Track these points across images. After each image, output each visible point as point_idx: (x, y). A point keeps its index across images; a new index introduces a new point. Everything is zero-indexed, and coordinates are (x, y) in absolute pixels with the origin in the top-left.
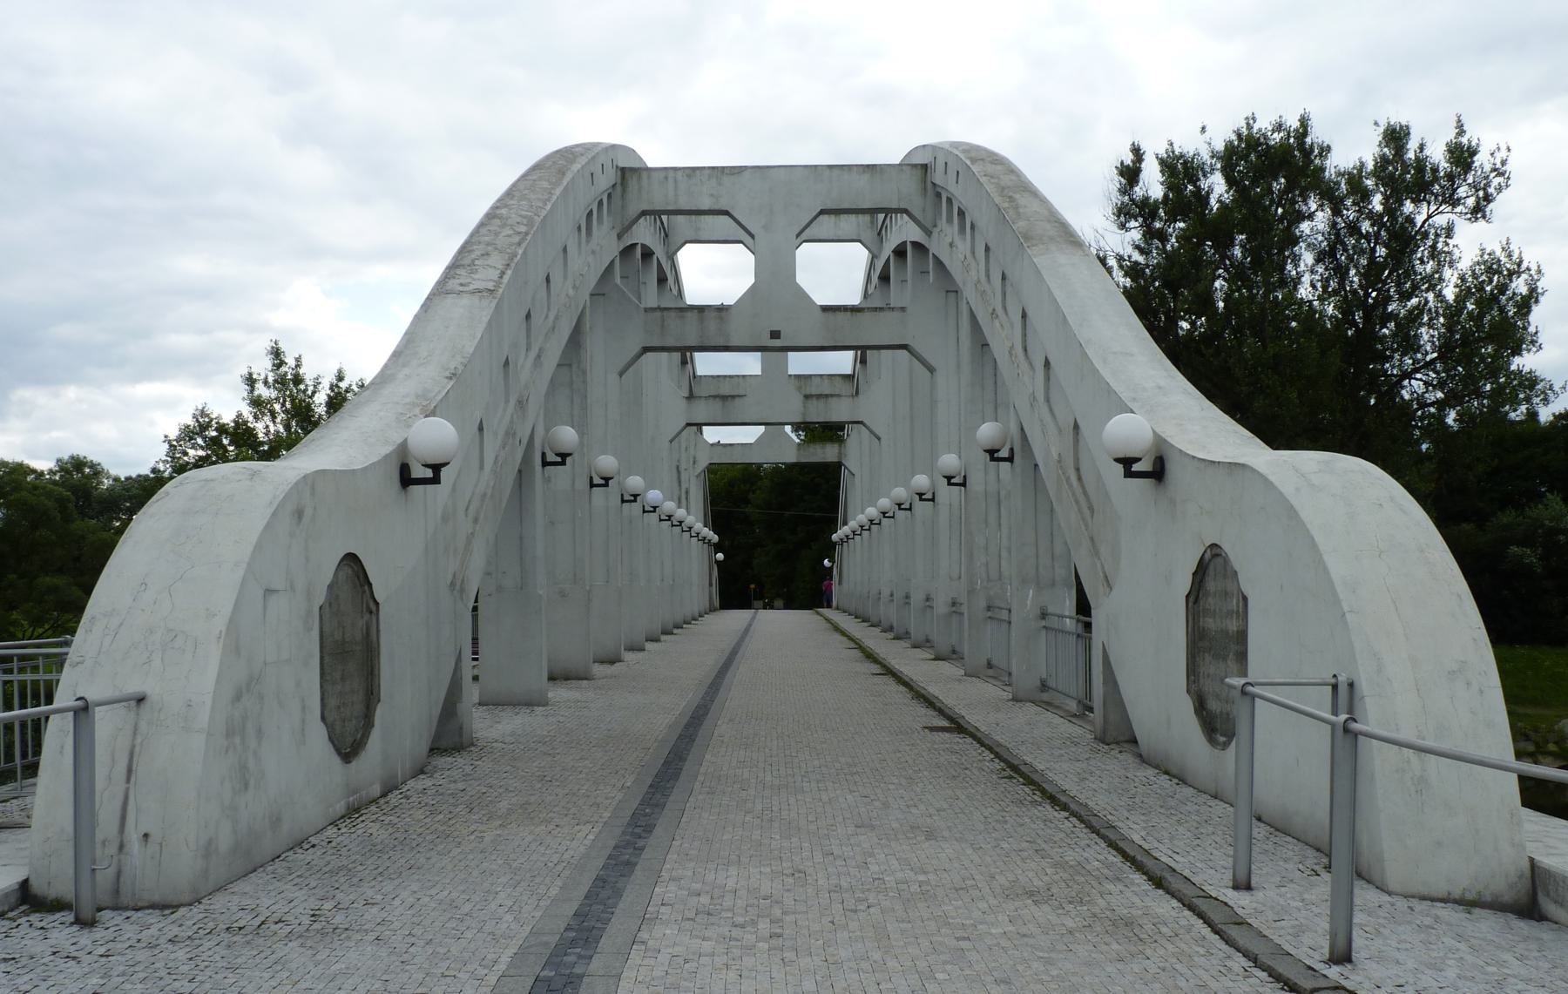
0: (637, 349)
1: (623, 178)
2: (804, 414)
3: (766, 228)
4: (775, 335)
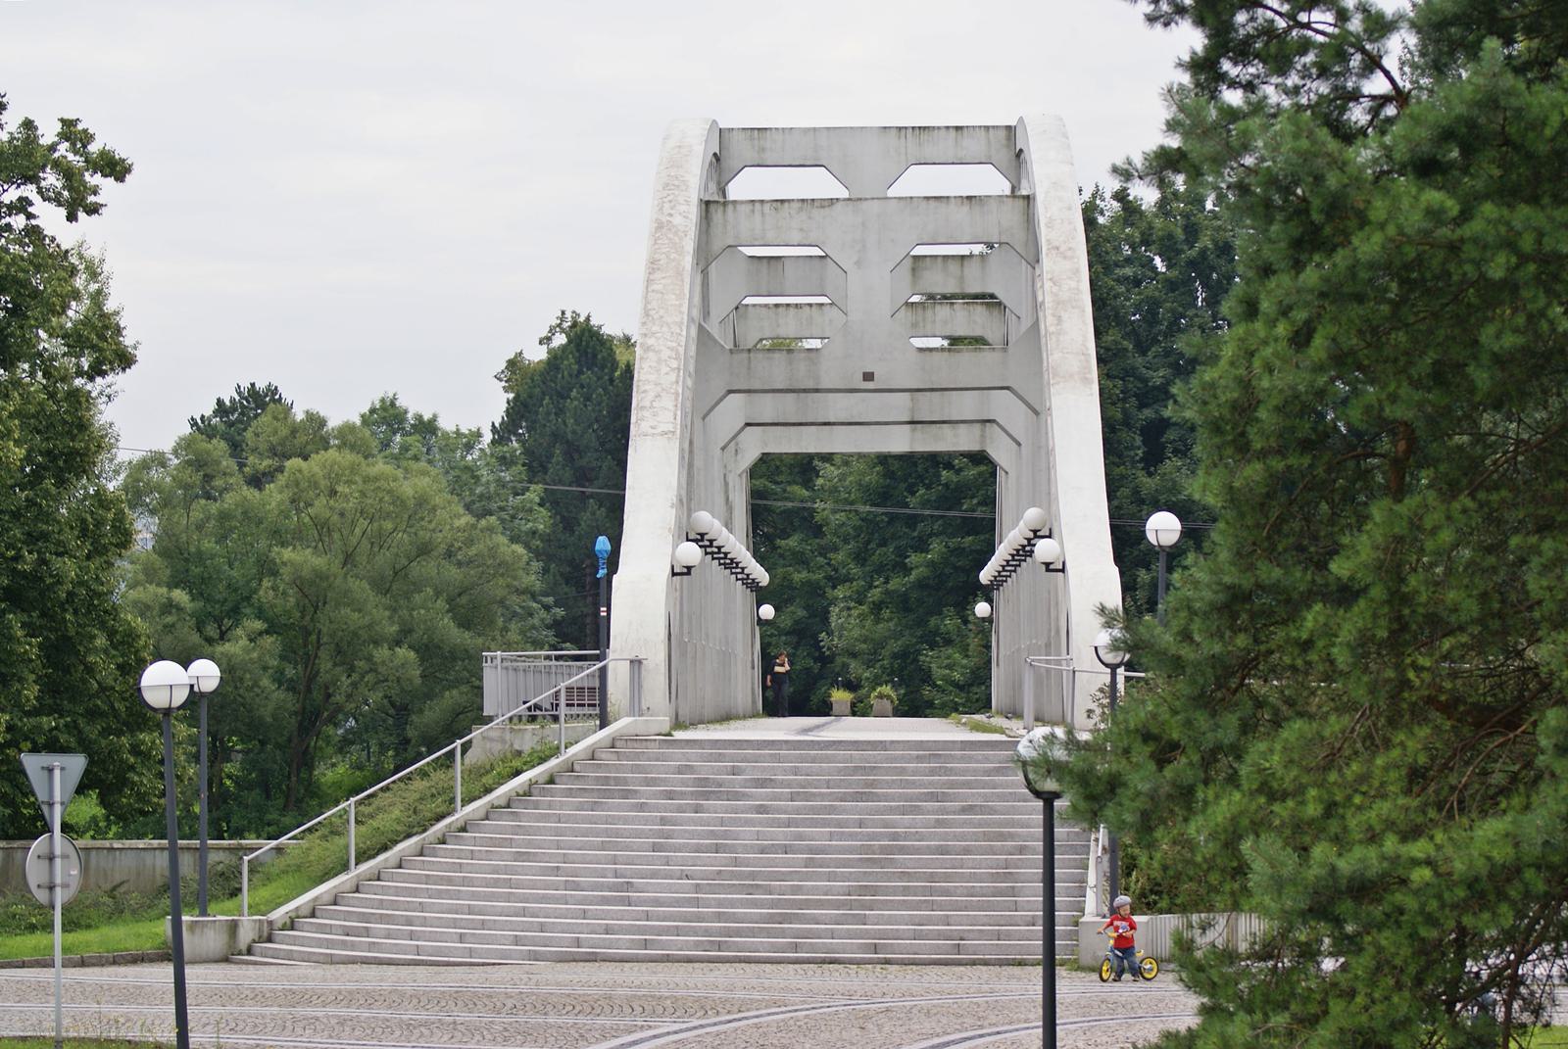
0: (724, 392)
1: (707, 211)
2: (912, 410)
3: (858, 263)
4: (868, 376)
